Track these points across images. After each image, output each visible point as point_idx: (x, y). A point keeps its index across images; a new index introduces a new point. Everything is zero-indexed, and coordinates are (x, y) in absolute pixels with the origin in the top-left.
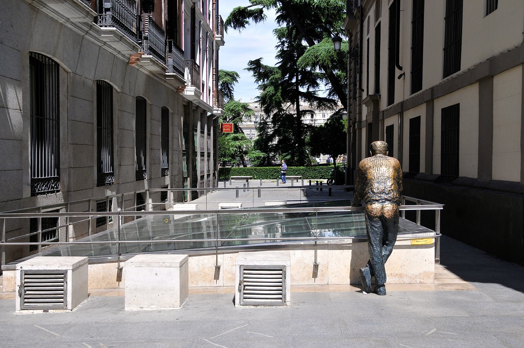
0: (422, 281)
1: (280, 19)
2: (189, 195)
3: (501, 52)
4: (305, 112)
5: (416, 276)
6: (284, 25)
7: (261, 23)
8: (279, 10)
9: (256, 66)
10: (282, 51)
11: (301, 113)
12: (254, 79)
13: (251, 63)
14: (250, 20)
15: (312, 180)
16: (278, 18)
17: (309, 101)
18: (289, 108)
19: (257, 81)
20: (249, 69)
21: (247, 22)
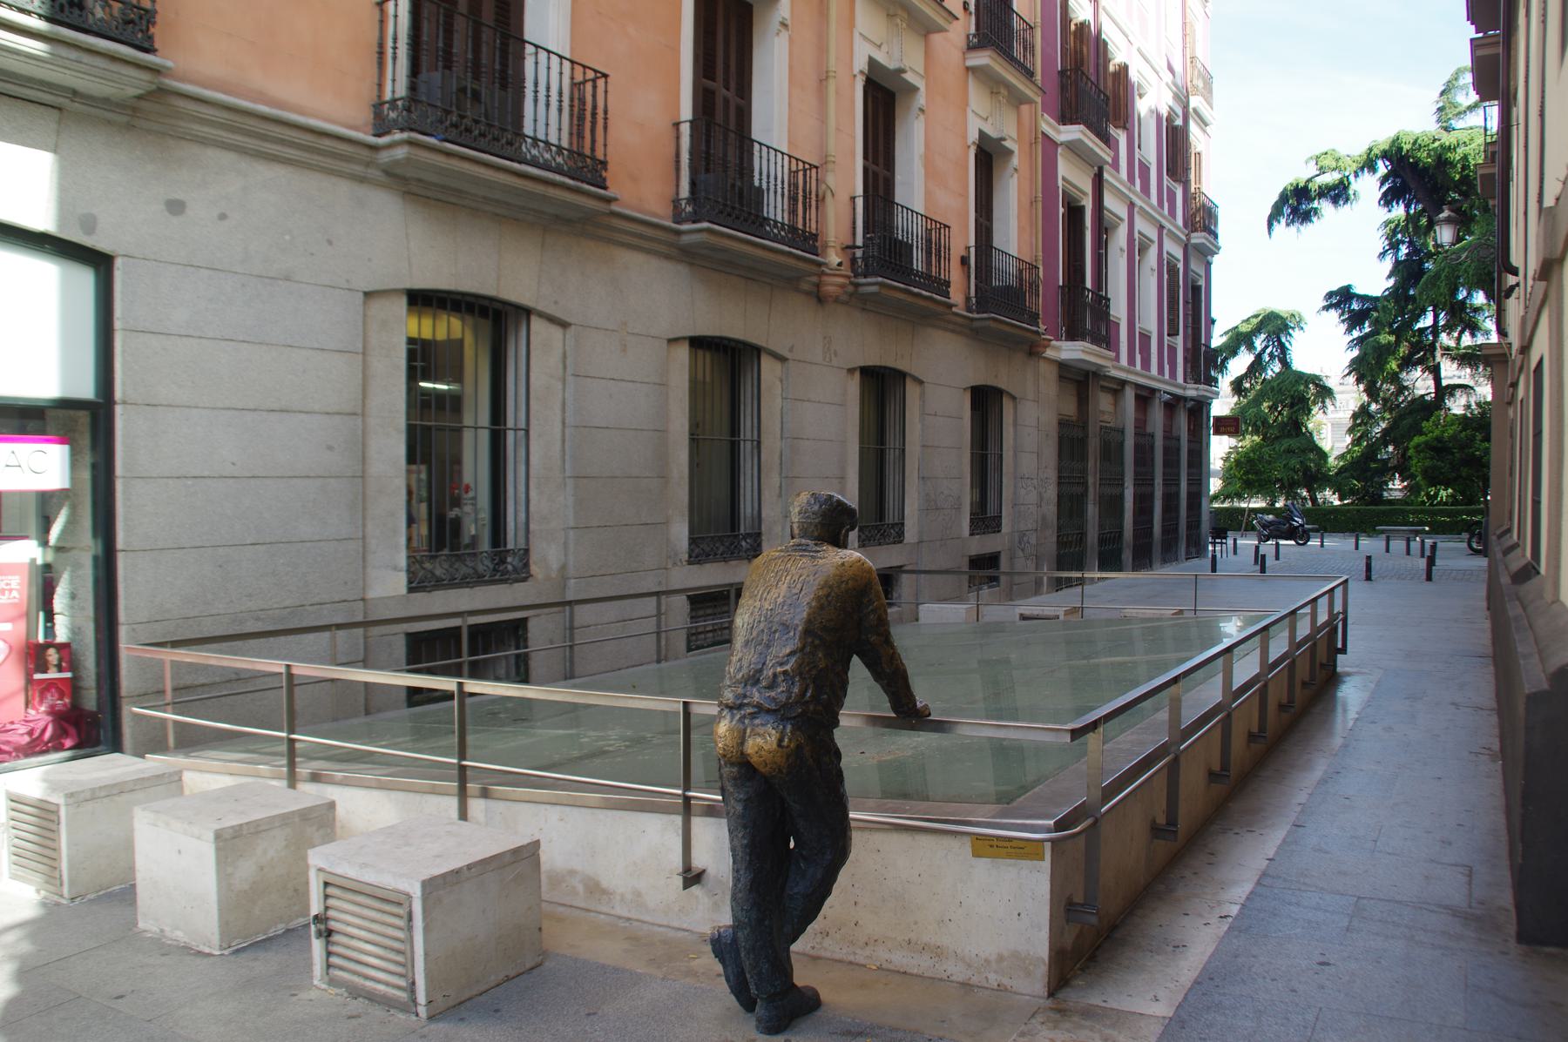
0: (1006, 981)
1: (1388, 199)
2: (1127, 556)
3: (1110, 47)
4: (1452, 389)
5: (987, 961)
6: (1399, 211)
7: (1345, 210)
8: (1384, 180)
9: (1341, 298)
10: (1397, 263)
11: (1444, 392)
12: (1343, 327)
13: (1330, 295)
14: (1325, 206)
15: (1282, 542)
16: (1385, 195)
17: (1470, 366)
18: (1420, 383)
19: (1349, 330)
20: (1326, 308)
21: (1316, 211)
